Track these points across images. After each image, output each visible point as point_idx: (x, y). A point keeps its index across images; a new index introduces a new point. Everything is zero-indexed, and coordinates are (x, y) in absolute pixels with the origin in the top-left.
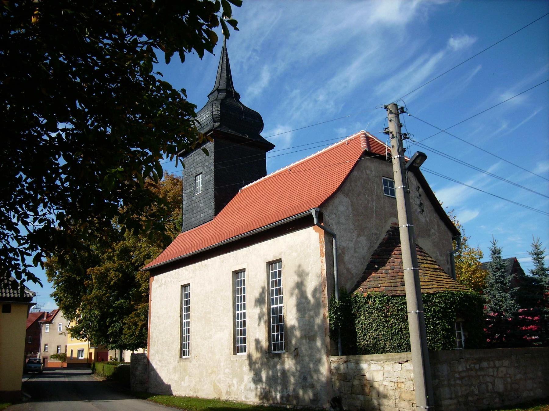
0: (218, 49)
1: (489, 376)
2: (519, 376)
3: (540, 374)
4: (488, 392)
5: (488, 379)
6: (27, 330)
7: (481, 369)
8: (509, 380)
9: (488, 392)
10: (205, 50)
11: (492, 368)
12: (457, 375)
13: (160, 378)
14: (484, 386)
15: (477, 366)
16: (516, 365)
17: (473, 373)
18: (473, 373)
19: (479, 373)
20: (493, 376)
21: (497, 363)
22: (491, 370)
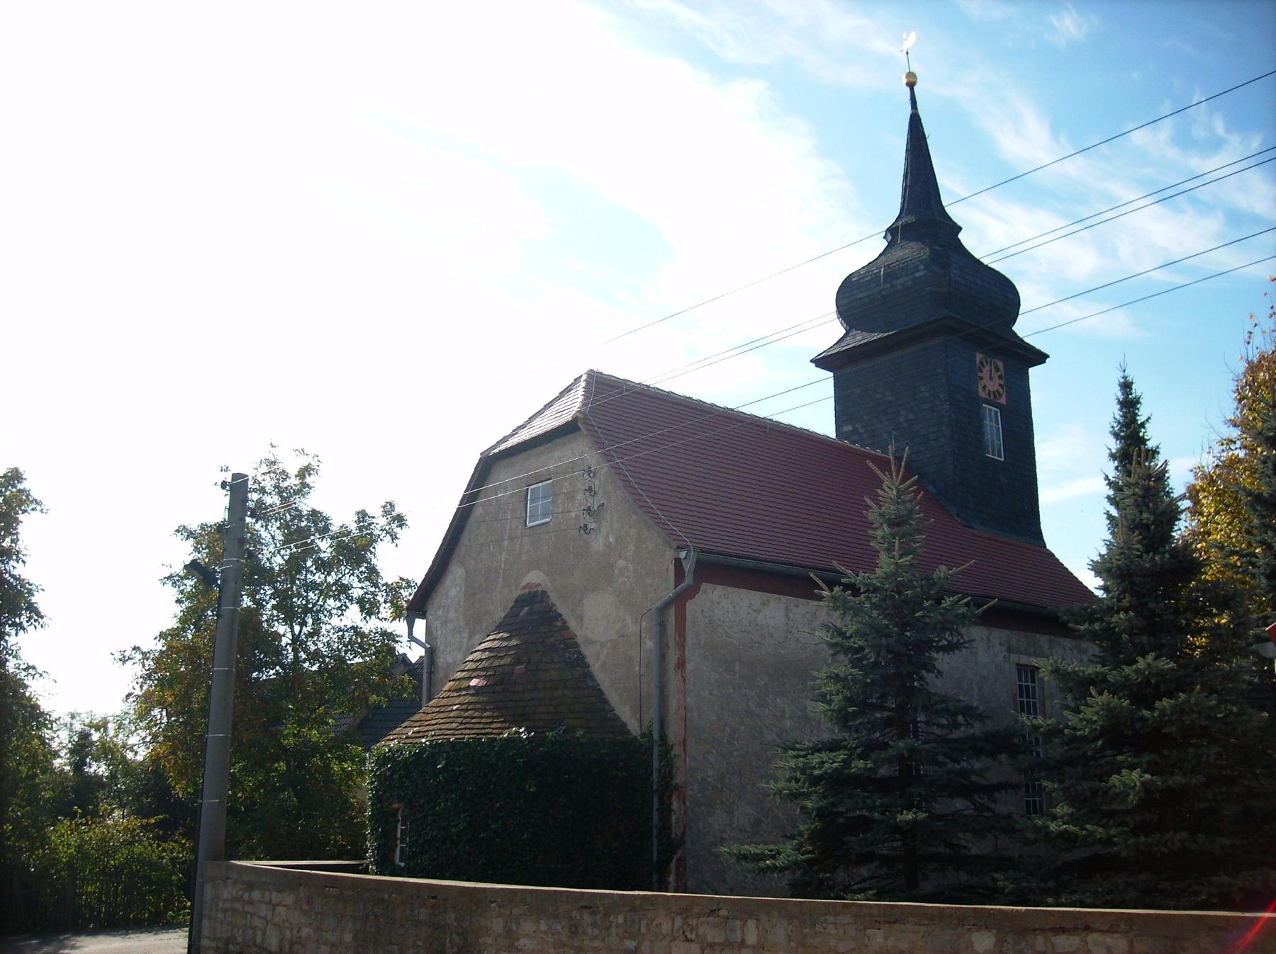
0: (1198, 163)
1: (259, 917)
2: (305, 931)
3: (348, 937)
4: (255, 945)
5: (258, 923)
6: (488, 465)
7: (251, 902)
8: (288, 932)
9: (255, 945)
10: (812, 408)
11: (266, 903)
12: (1165, 651)
13: (906, 159)
14: (250, 932)
15: (246, 896)
16: (305, 907)
17: (238, 906)
18: (238, 906)
19: (248, 908)
20: (264, 918)
21: (275, 897)
22: (264, 906)
